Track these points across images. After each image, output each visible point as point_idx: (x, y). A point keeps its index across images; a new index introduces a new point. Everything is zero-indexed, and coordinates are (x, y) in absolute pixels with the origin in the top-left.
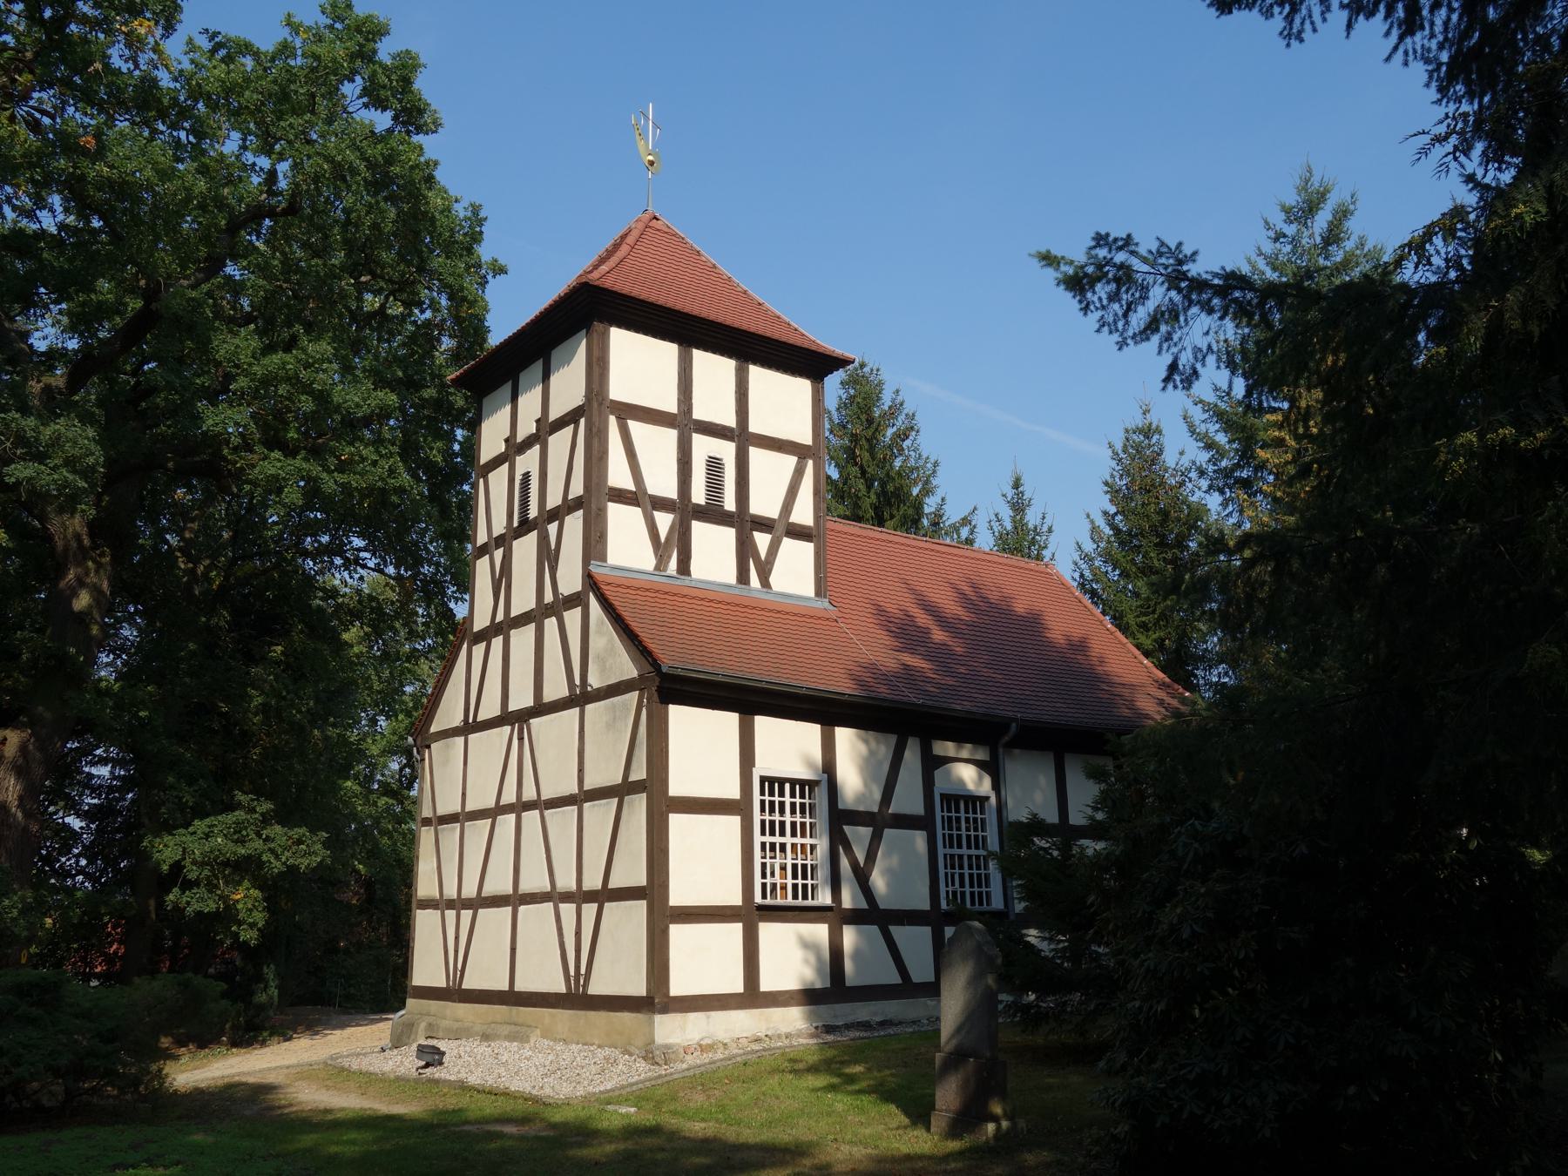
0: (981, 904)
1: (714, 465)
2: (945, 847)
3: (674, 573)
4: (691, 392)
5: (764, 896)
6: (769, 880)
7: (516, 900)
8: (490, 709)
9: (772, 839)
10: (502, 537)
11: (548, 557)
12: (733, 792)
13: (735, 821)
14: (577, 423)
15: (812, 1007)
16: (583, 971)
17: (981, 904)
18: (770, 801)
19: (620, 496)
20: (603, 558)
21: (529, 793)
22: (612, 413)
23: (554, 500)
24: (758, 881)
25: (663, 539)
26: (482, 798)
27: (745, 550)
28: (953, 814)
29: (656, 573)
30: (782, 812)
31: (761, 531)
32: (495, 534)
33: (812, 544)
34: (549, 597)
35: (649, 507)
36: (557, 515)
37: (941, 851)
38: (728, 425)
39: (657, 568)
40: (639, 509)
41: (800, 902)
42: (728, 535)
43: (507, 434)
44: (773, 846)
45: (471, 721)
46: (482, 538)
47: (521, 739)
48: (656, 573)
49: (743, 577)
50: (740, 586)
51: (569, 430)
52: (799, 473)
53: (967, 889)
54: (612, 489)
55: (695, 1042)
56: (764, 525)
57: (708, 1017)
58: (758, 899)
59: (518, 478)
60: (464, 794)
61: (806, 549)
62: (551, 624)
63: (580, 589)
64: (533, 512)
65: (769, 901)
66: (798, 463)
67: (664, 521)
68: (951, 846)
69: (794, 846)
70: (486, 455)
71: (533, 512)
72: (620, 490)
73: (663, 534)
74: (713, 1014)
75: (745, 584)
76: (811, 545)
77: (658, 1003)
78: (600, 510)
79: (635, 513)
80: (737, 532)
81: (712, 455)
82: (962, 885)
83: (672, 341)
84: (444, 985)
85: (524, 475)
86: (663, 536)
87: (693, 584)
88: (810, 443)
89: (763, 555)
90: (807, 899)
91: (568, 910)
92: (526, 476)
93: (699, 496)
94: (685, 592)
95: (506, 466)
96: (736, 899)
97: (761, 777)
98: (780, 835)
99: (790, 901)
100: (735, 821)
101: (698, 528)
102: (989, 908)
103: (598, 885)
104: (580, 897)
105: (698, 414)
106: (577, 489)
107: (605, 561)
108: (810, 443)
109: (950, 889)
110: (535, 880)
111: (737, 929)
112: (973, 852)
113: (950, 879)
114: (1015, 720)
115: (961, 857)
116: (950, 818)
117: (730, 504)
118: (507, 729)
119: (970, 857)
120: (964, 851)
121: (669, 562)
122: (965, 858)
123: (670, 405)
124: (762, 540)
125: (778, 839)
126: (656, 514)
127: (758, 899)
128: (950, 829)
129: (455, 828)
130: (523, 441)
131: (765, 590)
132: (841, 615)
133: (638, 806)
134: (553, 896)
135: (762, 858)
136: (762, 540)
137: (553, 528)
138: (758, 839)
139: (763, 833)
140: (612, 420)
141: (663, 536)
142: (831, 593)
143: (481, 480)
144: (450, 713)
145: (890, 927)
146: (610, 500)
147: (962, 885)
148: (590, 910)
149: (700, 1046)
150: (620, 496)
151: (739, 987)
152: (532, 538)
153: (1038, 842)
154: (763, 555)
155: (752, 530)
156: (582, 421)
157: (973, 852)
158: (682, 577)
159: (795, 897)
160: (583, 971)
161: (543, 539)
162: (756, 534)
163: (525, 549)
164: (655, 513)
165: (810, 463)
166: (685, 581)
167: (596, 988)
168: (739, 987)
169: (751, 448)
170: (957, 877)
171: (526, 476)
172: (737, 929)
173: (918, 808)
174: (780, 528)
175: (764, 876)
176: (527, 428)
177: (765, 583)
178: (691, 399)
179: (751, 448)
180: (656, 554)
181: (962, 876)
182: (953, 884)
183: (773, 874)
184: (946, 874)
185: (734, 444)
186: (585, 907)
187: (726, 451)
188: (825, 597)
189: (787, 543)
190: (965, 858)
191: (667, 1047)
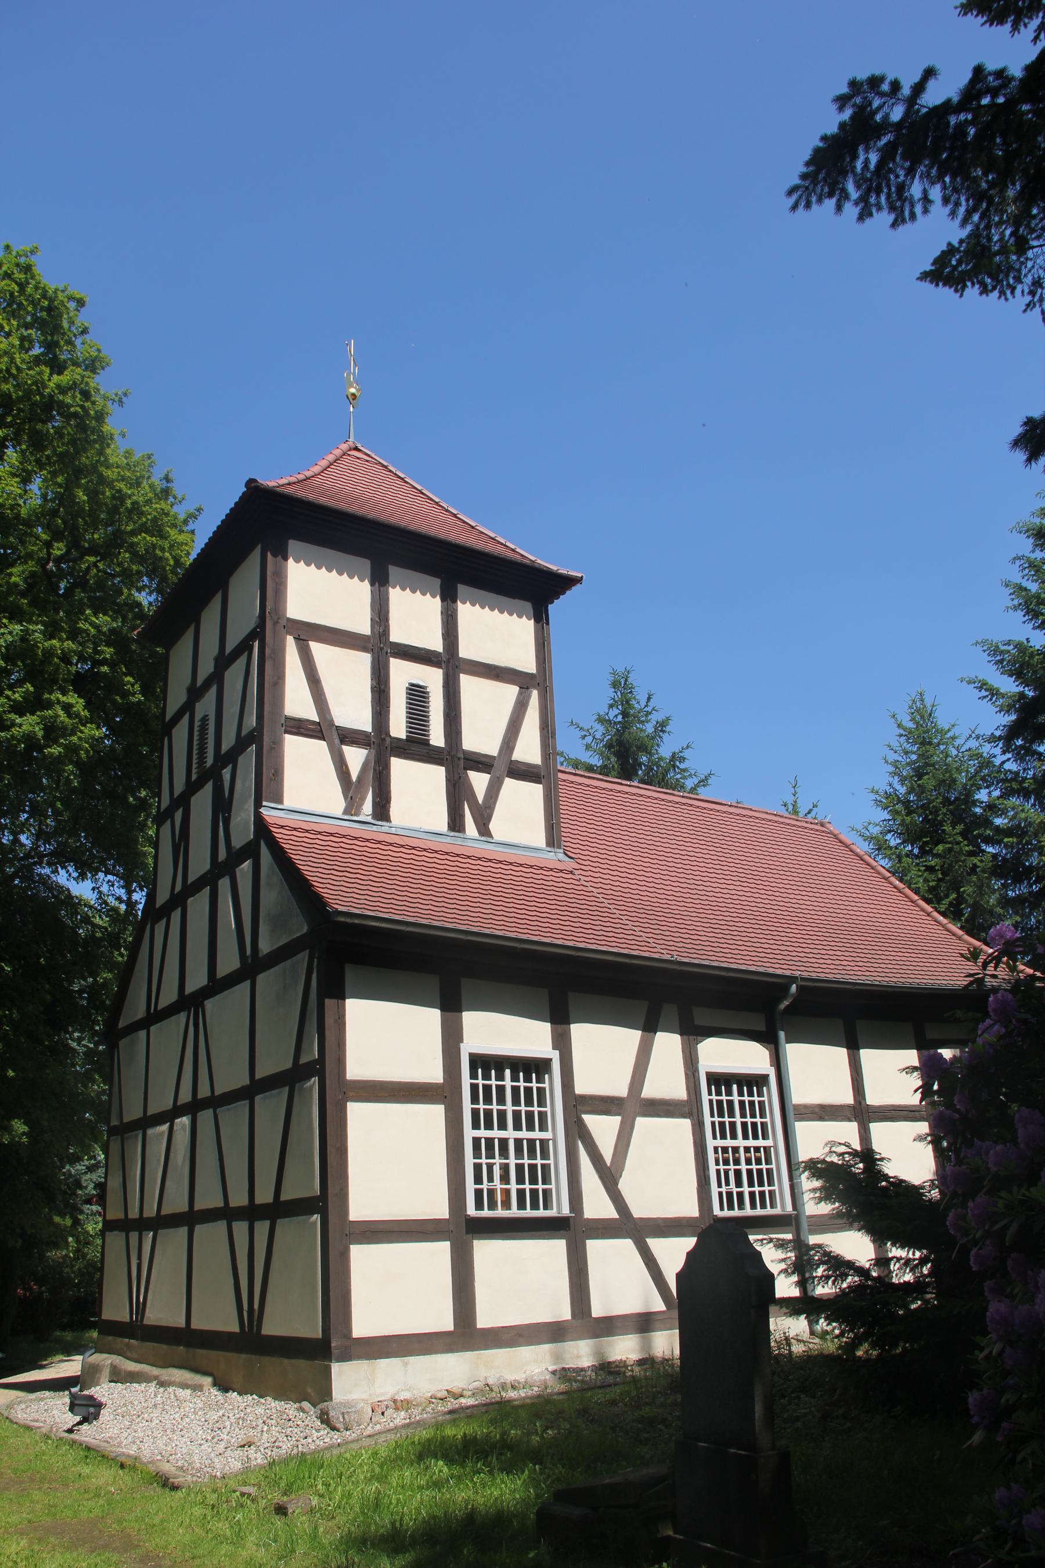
1: (417, 695)
2: (715, 1137)
3: (369, 819)
4: (388, 612)
5: (479, 1205)
6: (485, 1186)
7: (191, 1218)
8: (168, 996)
9: (489, 1134)
11: (222, 806)
12: (434, 1073)
13: (437, 1112)
16: (256, 1306)
19: (300, 727)
20: (278, 798)
21: (204, 1092)
24: (470, 1187)
26: (163, 1102)
28: (724, 1098)
29: (346, 817)
30: (501, 1100)
33: (541, 786)
34: (222, 855)
35: (337, 741)
37: (711, 1143)
39: (345, 812)
40: (324, 743)
41: (528, 1213)
42: (436, 775)
49: (456, 824)
50: (452, 834)
52: (520, 707)
55: (388, 1397)
56: (481, 763)
57: (406, 1364)
58: (471, 1210)
62: (224, 884)
65: (486, 1213)
66: (520, 694)
67: (356, 757)
68: (723, 1137)
69: (518, 1142)
70: (171, 709)
72: (300, 720)
73: (354, 773)
74: (412, 1359)
75: (459, 831)
76: (540, 787)
77: (336, 1348)
78: (274, 743)
79: (320, 747)
80: (447, 771)
82: (739, 1184)
84: (127, 1319)
86: (354, 775)
87: (393, 831)
88: (534, 672)
89: (480, 798)
91: (241, 1228)
92: (204, 719)
93: (398, 727)
94: (381, 837)
96: (441, 1210)
97: (471, 1055)
99: (514, 1212)
100: (437, 1112)
101: (398, 766)
104: (252, 1213)
107: (281, 802)
108: (534, 672)
109: (724, 1189)
110: (209, 1199)
111: (443, 1249)
112: (524, 1134)
113: (723, 1178)
114: (792, 979)
116: (720, 1103)
117: (437, 737)
118: (182, 1016)
120: (740, 1142)
121: (362, 805)
122: (742, 1150)
123: (364, 627)
124: (479, 781)
125: (496, 1133)
127: (471, 1210)
128: (721, 1114)
129: (137, 1136)
131: (483, 838)
132: (578, 867)
134: (227, 1214)
136: (479, 781)
137: (226, 774)
138: (469, 1134)
139: (476, 1125)
140: (290, 642)
141: (354, 775)
142: (565, 844)
143: (166, 739)
144: (136, 1008)
145: (648, 1240)
146: (286, 732)
147: (739, 1184)
149: (395, 1401)
150: (300, 727)
151: (445, 1322)
153: (1011, 193)
154: (480, 798)
155: (466, 769)
157: (524, 1134)
158: (380, 823)
159: (521, 1205)
160: (256, 1306)
161: (218, 790)
164: (344, 747)
165: (535, 694)
166: (385, 827)
167: (272, 1327)
168: (445, 1322)
169: (461, 675)
170: (497, 1172)
171: (204, 719)
172: (443, 1249)
173: (679, 1091)
174: (500, 767)
175: (478, 1180)
176: (206, 668)
177: (484, 829)
178: (387, 620)
179: (461, 675)
181: (738, 1173)
182: (727, 1183)
183: (491, 1179)
184: (718, 1171)
185: (441, 671)
187: (432, 678)
188: (559, 847)
189: (509, 784)
190: (742, 1150)
191: (347, 1404)
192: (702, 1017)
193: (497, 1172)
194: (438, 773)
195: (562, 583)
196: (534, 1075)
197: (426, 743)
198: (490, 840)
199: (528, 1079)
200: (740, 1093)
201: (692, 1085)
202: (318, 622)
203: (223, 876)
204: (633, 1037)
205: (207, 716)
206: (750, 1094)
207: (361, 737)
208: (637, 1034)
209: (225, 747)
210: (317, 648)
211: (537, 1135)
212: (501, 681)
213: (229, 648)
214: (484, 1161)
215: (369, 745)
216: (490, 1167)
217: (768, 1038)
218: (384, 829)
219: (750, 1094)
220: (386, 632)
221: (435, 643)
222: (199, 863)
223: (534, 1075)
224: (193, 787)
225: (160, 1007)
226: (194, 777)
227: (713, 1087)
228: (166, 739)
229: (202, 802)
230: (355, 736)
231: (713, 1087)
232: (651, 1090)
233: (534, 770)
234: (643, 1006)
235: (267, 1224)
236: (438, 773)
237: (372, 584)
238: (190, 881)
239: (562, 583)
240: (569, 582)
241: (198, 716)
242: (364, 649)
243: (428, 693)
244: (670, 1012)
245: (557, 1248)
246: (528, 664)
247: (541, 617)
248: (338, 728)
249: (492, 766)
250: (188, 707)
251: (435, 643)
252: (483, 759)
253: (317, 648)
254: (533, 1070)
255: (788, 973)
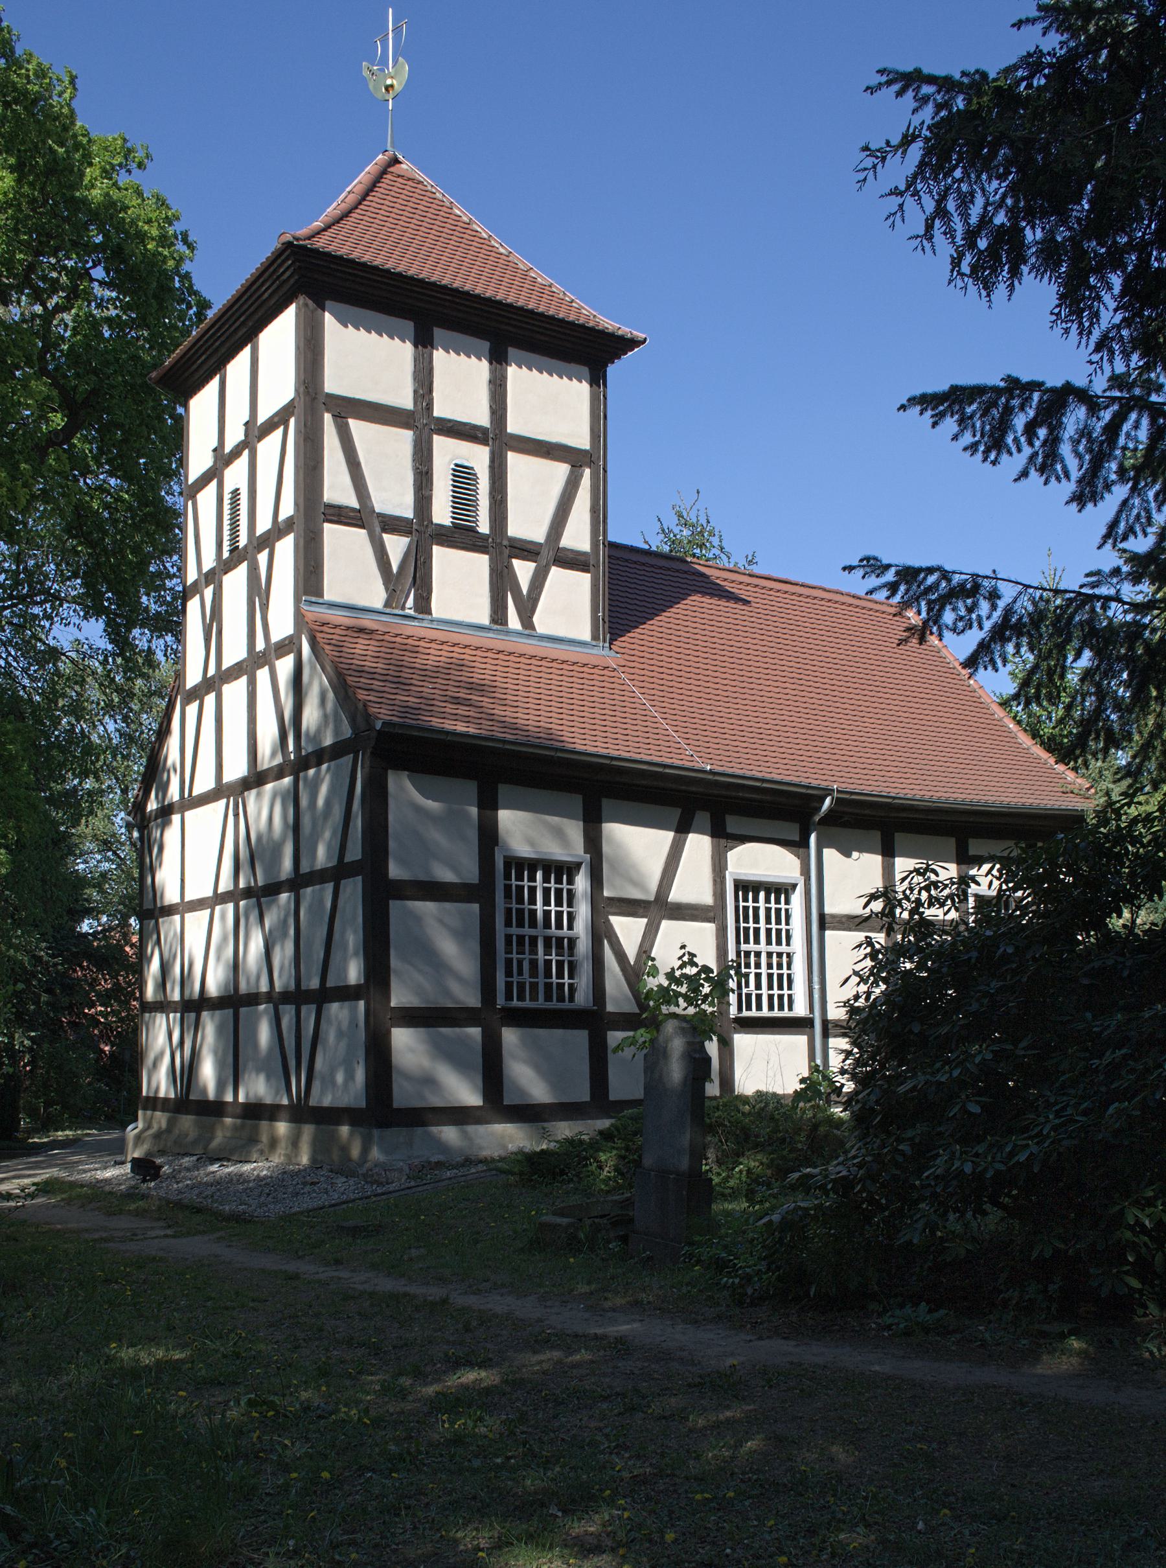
0: (781, 1008)
1: (463, 476)
3: (411, 612)
6: (776, 992)
10: (212, 572)
11: (258, 592)
14: (286, 423)
15: (293, 1125)
17: (781, 1008)
18: (780, 903)
19: (340, 515)
22: (328, 411)
23: (264, 524)
25: (395, 569)
27: (501, 581)
29: (388, 610)
31: (524, 559)
32: (205, 569)
34: (260, 645)
35: (378, 529)
36: (267, 541)
38: (479, 423)
39: (387, 604)
40: (363, 532)
43: (215, 444)
44: (521, 939)
45: (186, 796)
46: (192, 576)
47: (236, 815)
48: (388, 610)
49: (498, 615)
51: (278, 433)
53: (764, 991)
54: (329, 506)
56: (526, 550)
58: (501, 1001)
59: (227, 497)
60: (183, 880)
61: (582, 581)
62: (263, 675)
63: (292, 632)
64: (243, 541)
66: (572, 472)
67: (396, 546)
71: (243, 541)
75: (501, 624)
80: (491, 560)
81: (459, 462)
82: (758, 986)
83: (584, 365)
85: (232, 493)
90: (751, 1010)
92: (236, 493)
93: (442, 513)
95: (214, 484)
98: (517, 926)
101: (439, 553)
102: (791, 1014)
103: (315, 983)
105: (512, 427)
106: (287, 509)
107: (322, 596)
114: (828, 792)
115: (758, 954)
117: (484, 527)
119: (770, 955)
123: (404, 399)
124: (523, 570)
126: (386, 537)
130: (231, 451)
133: (353, 888)
135: (506, 953)
136: (523, 570)
137: (263, 558)
140: (327, 417)
143: (190, 503)
148: (309, 1013)
150: (340, 515)
152: (242, 569)
155: (511, 557)
156: (292, 421)
157: (774, 948)
158: (420, 616)
162: (515, 562)
163: (236, 582)
164: (385, 536)
165: (587, 472)
170: (526, 966)
171: (236, 493)
175: (509, 973)
176: (236, 433)
180: (387, 589)
181: (758, 976)
183: (520, 973)
186: (304, 1009)
187: (478, 457)
189: (555, 571)
192: (733, 824)
193: (526, 966)
194: (482, 561)
195: (621, 345)
196: (565, 877)
197: (473, 530)
198: (533, 633)
199: (559, 881)
200: (768, 901)
201: (719, 891)
202: (357, 397)
203: (261, 666)
204: (666, 837)
205: (238, 489)
206: (778, 901)
207: (403, 524)
208: (670, 835)
209: (259, 530)
210: (356, 426)
211: (784, 948)
212: (552, 459)
213: (262, 417)
214: (515, 956)
215: (411, 533)
216: (520, 962)
217: (798, 845)
218: (425, 624)
219: (778, 901)
220: (429, 407)
221: (481, 417)
222: (234, 651)
223: (565, 877)
224: (225, 566)
225: (195, 793)
226: (226, 555)
227: (740, 893)
228: (190, 503)
229: (236, 582)
230: (398, 523)
231: (740, 893)
232: (677, 894)
233: (582, 558)
234: (676, 813)
235: (314, 1007)
236: (482, 561)
237: (416, 346)
238: (224, 667)
239: (621, 345)
240: (633, 343)
241: (228, 488)
242: (406, 425)
243: (475, 475)
244: (703, 817)
245: (580, 1038)
246: (581, 440)
247: (597, 379)
248: (380, 515)
249: (538, 554)
250: (214, 474)
251: (481, 417)
252: (529, 547)
253: (356, 426)
254: (565, 872)
255: (824, 784)
